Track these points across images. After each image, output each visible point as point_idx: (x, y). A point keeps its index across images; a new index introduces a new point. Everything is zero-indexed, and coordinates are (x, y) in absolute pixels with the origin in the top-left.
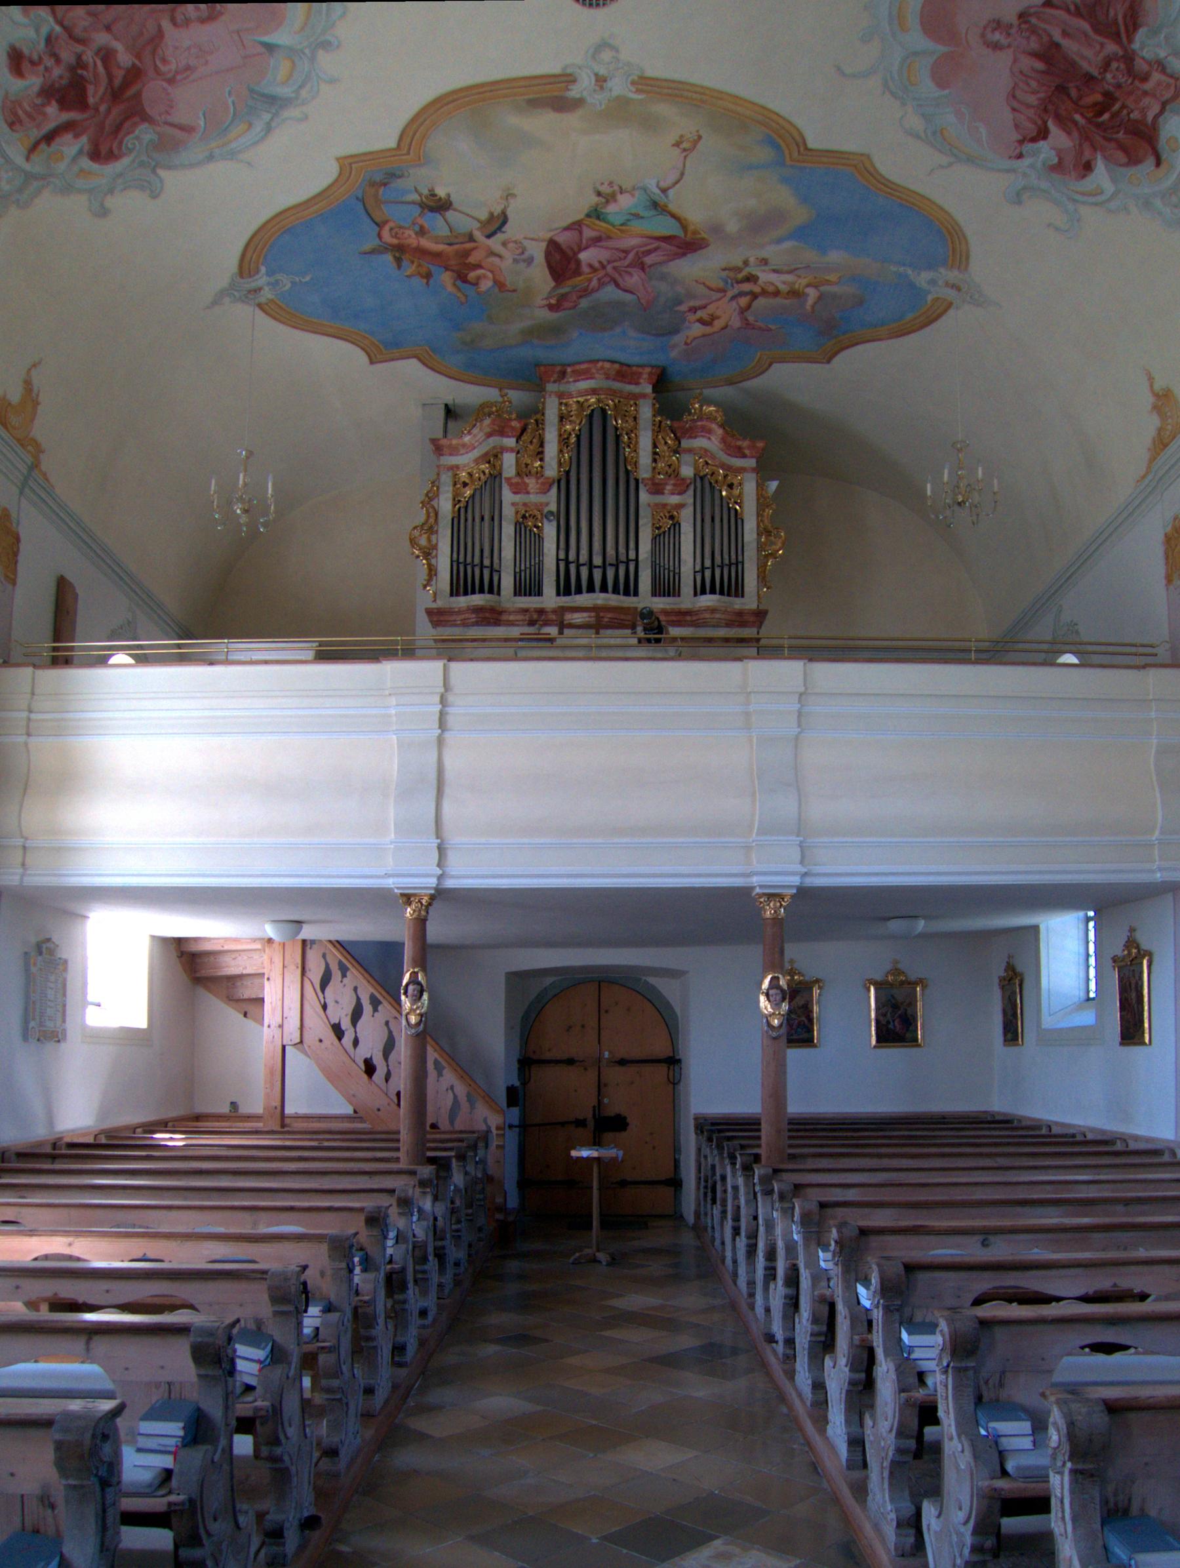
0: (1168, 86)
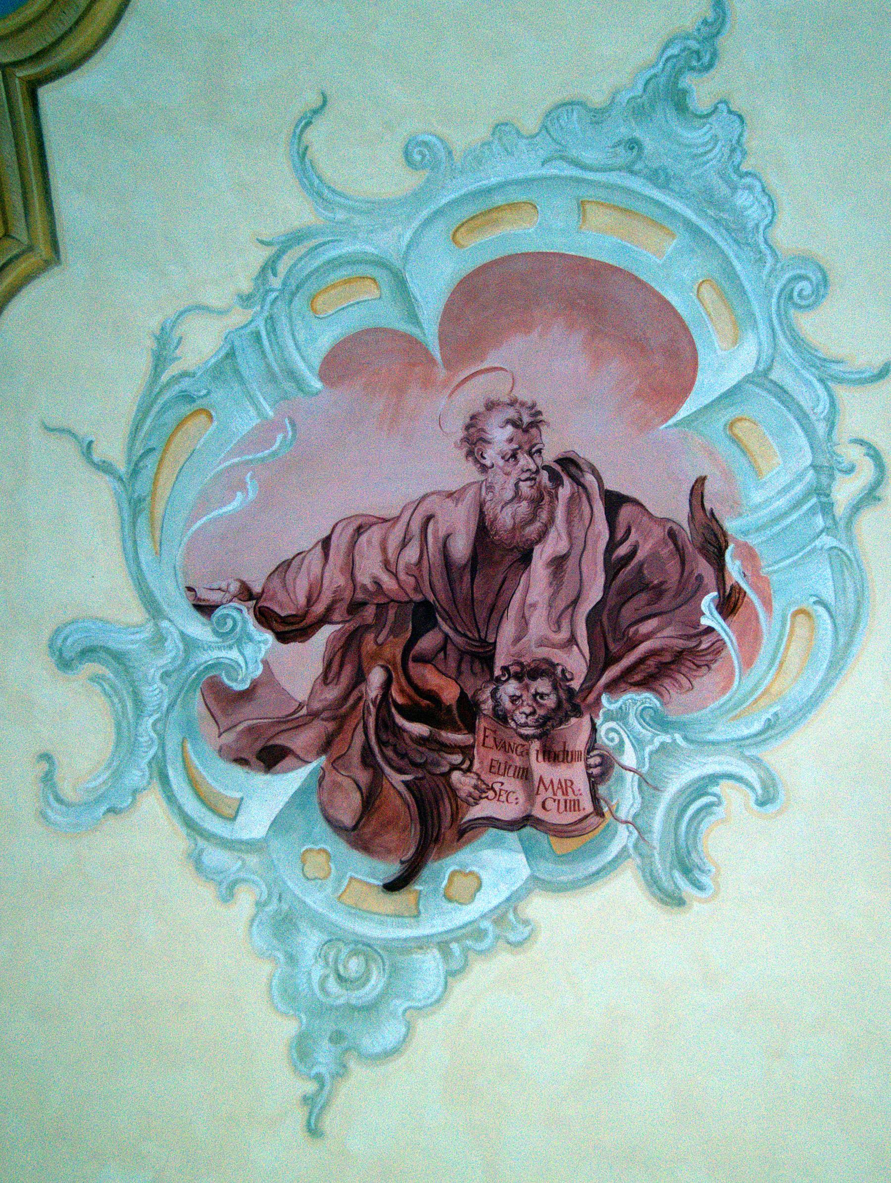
0: (575, 805)
